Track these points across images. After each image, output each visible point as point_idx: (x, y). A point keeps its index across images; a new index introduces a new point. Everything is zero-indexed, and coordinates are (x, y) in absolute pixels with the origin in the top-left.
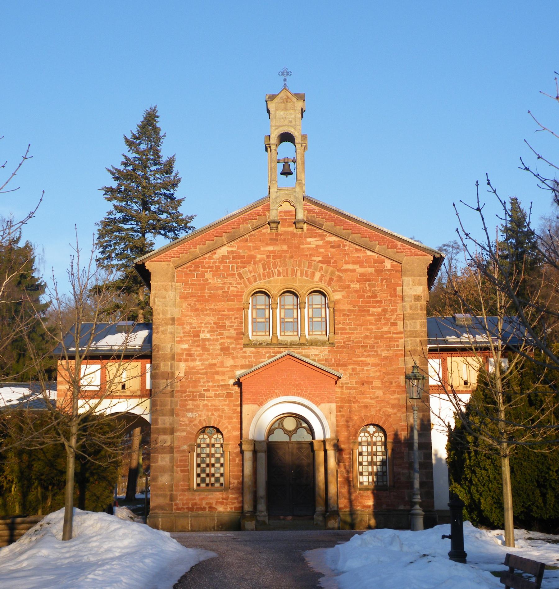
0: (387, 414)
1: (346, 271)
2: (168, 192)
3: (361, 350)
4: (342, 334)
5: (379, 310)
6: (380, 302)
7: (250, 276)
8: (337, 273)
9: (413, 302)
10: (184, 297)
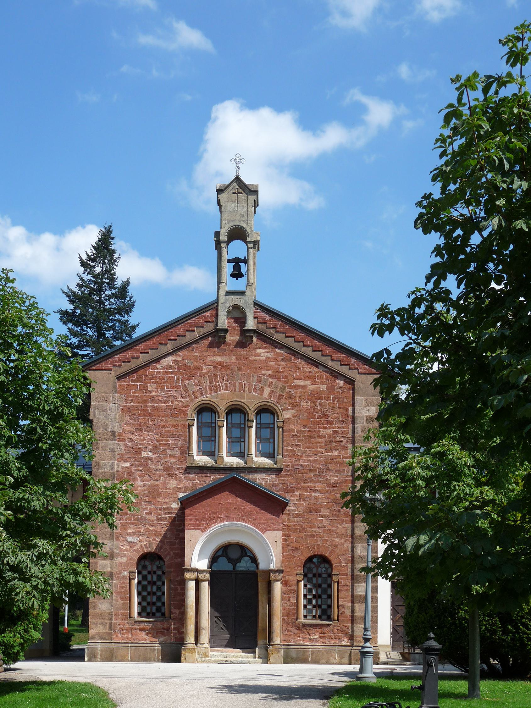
0: (334, 543)
1: (297, 387)
2: (123, 319)
3: (310, 474)
4: (290, 456)
5: (330, 431)
6: (330, 423)
7: (196, 388)
8: (287, 389)
9: (365, 424)
10: (126, 410)
